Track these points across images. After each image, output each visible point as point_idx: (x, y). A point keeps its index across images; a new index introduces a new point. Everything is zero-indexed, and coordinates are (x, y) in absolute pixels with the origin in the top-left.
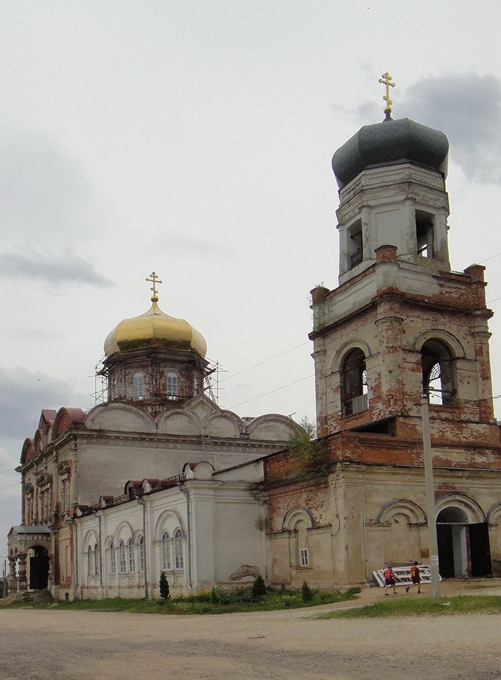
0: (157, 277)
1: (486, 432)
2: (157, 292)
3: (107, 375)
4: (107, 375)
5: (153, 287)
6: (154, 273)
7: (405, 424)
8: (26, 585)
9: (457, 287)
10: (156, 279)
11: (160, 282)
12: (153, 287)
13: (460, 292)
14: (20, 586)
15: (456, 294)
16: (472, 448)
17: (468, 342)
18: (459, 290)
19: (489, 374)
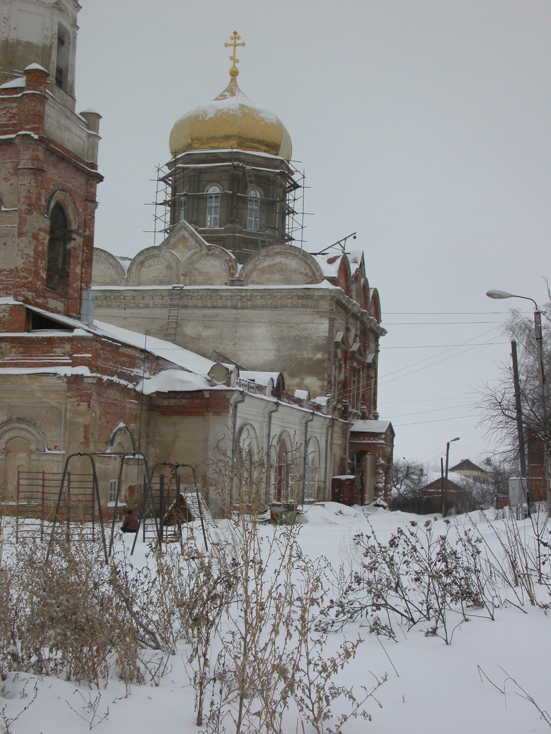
0: (239, 38)
1: (4, 316)
2: (237, 61)
3: (170, 182)
4: (170, 182)
5: (232, 55)
6: (235, 33)
7: (189, 297)
8: (397, 491)
9: (6, 107)
10: (238, 42)
11: (243, 45)
12: (232, 55)
13: (11, 113)
14: (282, 466)
15: (4, 117)
16: (6, 342)
17: (12, 184)
18: (10, 111)
19: (91, 225)
